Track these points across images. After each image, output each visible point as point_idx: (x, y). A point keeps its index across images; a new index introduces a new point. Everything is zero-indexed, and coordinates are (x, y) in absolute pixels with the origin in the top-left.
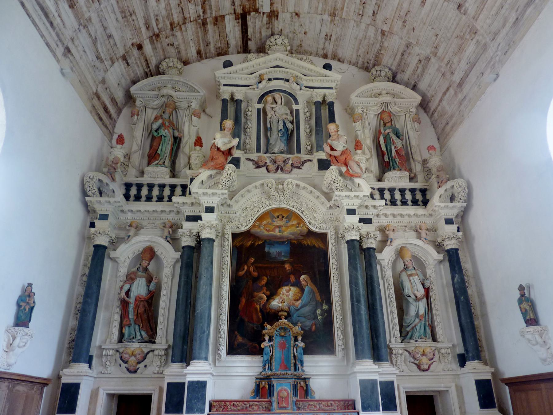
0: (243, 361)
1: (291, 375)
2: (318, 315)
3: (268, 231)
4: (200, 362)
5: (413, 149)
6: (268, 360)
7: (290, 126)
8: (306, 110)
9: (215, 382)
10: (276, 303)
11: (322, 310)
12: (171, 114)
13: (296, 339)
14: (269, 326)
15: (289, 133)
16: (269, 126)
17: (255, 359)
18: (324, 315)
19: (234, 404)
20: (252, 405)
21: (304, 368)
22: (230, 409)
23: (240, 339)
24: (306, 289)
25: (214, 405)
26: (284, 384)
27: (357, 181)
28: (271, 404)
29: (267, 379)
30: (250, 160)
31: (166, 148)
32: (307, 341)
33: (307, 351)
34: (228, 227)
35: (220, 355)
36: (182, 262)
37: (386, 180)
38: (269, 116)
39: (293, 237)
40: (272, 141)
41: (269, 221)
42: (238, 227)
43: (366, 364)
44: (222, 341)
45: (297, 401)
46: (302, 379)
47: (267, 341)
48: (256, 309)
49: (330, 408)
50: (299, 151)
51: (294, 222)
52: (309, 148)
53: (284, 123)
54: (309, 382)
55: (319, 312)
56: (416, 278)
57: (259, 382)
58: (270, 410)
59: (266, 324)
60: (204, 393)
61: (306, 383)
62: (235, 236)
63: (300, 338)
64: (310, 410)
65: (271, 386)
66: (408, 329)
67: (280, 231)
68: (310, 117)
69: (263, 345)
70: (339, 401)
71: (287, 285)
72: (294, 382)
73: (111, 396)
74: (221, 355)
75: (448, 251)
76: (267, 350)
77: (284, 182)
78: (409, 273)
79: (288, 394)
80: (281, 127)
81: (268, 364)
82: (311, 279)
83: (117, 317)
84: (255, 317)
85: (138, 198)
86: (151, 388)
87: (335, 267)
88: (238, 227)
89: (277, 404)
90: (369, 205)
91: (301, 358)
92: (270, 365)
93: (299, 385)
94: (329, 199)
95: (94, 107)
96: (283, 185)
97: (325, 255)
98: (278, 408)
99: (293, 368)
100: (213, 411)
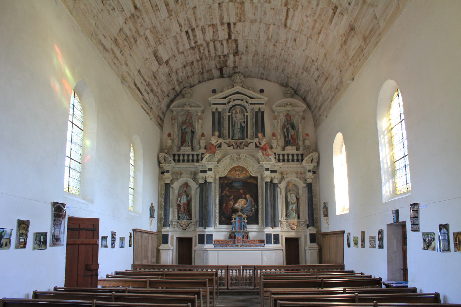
3: (234, 176)
5: (300, 134)
7: (243, 125)
8: (251, 114)
10: (237, 206)
11: (254, 208)
12: (190, 120)
13: (244, 219)
14: (234, 215)
15: (243, 128)
16: (234, 125)
21: (247, 229)
23: (223, 219)
24: (249, 200)
27: (270, 157)
30: (225, 143)
31: (188, 137)
33: (248, 223)
34: (217, 175)
35: (216, 225)
36: (200, 189)
37: (286, 150)
38: (234, 120)
39: (244, 179)
40: (235, 132)
41: (234, 172)
42: (221, 175)
45: (244, 240)
48: (229, 208)
50: (247, 137)
51: (244, 172)
52: (252, 134)
53: (241, 124)
56: (293, 195)
59: (233, 214)
62: (220, 178)
65: (235, 235)
66: (289, 214)
67: (239, 176)
68: (253, 118)
70: (259, 240)
71: (241, 199)
73: (177, 238)
75: (308, 184)
77: (240, 154)
78: (291, 192)
80: (239, 126)
82: (251, 196)
83: (176, 210)
84: (229, 211)
85: (179, 161)
86: (192, 235)
87: (260, 191)
88: (221, 175)
90: (276, 165)
94: (259, 163)
95: (158, 122)
96: (240, 156)
97: (257, 185)
99: (243, 229)
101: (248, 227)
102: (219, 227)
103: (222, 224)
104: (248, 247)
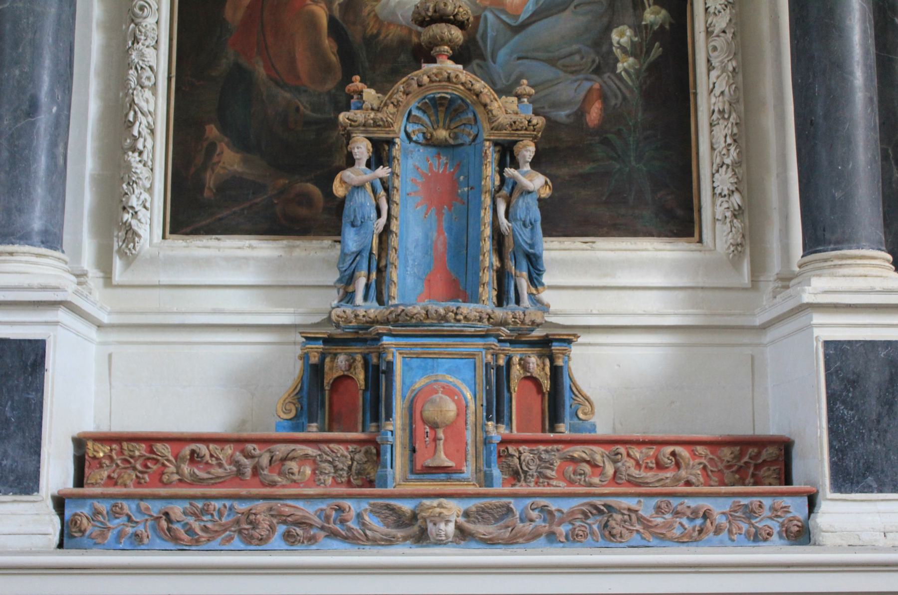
0: (247, 259)
1: (480, 320)
2: (618, 52)
4: (11, 254)
6: (366, 254)
9: (110, 356)
11: (638, 28)
14: (370, 94)
17: (303, 254)
18: (648, 52)
19: (193, 452)
20: (284, 459)
21: (546, 296)
22: (176, 477)
25: (94, 458)
26: (446, 363)
28: (378, 454)
29: (364, 341)
32: (564, 172)
35: (130, 234)
43: (861, 271)
44: (140, 170)
45: (505, 442)
46: (532, 344)
47: (361, 166)
48: (312, 22)
49: (669, 474)
54: (566, 355)
55: (624, 40)
57: (323, 356)
58: (371, 483)
60: (32, 395)
61: (552, 361)
63: (528, 151)
64: (571, 482)
69: (343, 182)
72: (496, 356)
74: (135, 234)
76: (364, 202)
79: (462, 410)
81: (364, 272)
89: (408, 452)
91: (532, 246)
92: (374, 276)
93: (516, 371)
98: (413, 471)
99: (489, 293)
100: (93, 485)
101: (563, 264)
102: (170, 263)
103: (196, 232)
104: (573, 538)
